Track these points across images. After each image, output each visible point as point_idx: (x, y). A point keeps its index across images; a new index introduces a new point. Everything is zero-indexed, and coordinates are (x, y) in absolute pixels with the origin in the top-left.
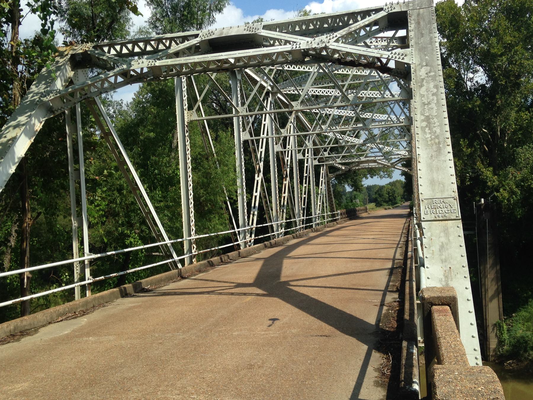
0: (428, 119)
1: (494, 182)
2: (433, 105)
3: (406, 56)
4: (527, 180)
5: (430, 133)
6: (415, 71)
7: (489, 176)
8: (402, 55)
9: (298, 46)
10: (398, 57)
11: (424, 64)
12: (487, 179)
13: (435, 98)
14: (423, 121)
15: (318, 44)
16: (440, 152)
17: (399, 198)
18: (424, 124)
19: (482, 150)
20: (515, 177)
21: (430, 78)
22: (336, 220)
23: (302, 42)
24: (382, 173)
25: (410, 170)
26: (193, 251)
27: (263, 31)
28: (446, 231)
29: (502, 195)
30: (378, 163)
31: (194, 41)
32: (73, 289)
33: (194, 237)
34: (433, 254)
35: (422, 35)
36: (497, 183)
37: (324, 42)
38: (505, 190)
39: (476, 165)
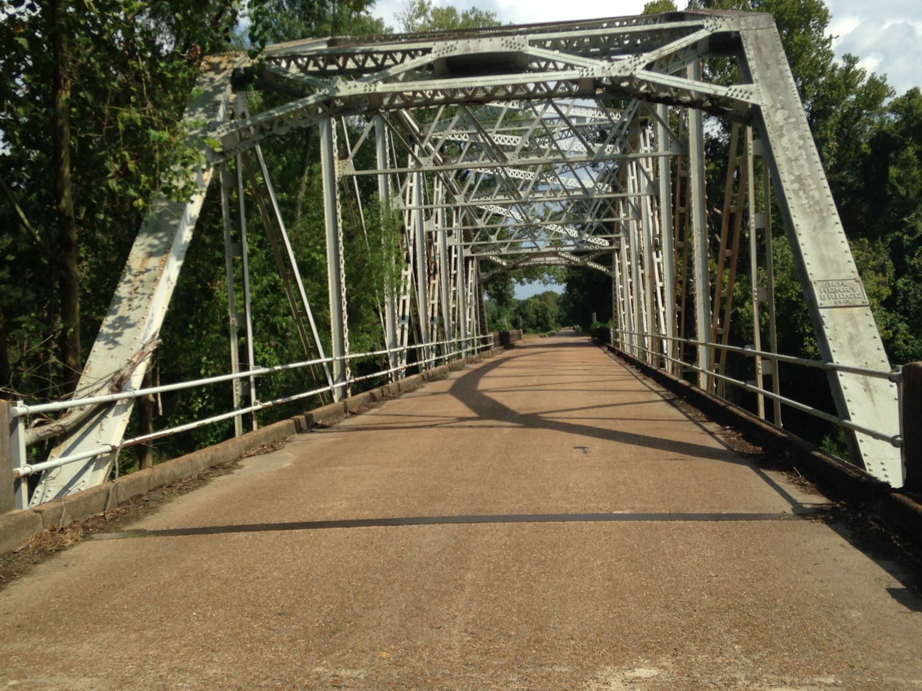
0: (799, 179)
2: (803, 162)
3: (751, 93)
5: (807, 198)
6: (768, 115)
8: (746, 92)
9: (590, 74)
10: (740, 95)
11: (779, 106)
13: (804, 153)
14: (793, 182)
15: (620, 72)
16: (824, 223)
17: (552, 321)
18: (796, 186)
21: (792, 126)
22: (487, 348)
23: (595, 67)
24: (546, 276)
25: (611, 270)
26: (348, 378)
27: (530, 48)
28: (852, 319)
30: (560, 256)
31: (429, 58)
32: (232, 419)
33: (254, 371)
34: (841, 346)
35: (768, 67)
37: (627, 69)
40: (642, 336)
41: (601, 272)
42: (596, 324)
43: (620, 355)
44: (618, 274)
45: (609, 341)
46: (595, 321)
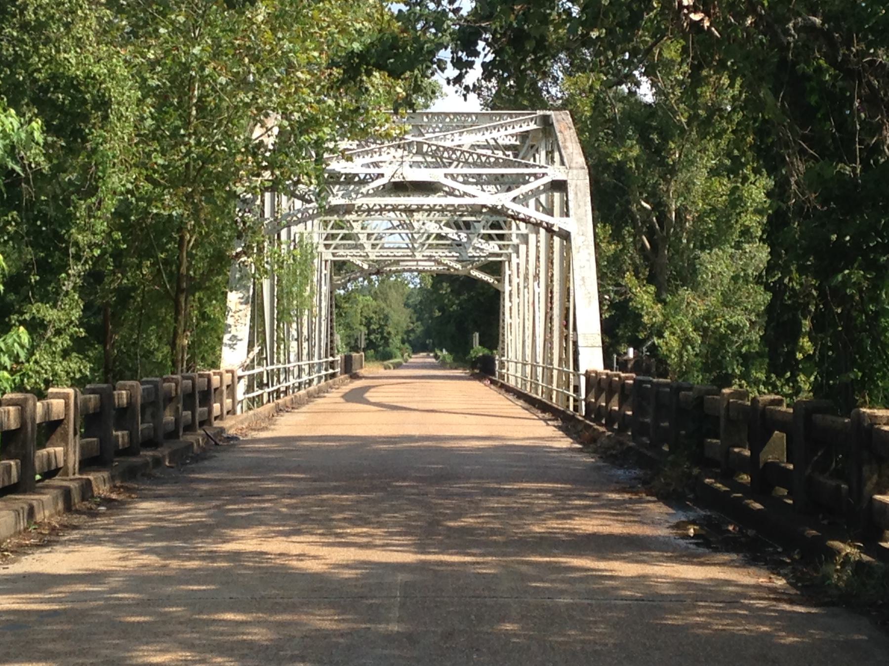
1: (655, 316)
4: (716, 317)
7: (647, 303)
12: (642, 309)
17: (395, 341)
19: (639, 246)
20: (694, 310)
22: (333, 376)
25: (499, 281)
29: (667, 343)
36: (660, 318)
38: (673, 334)
39: (623, 278)
40: (534, 367)
41: (487, 283)
42: (478, 350)
43: (508, 390)
44: (507, 288)
45: (494, 375)
46: (125, 396)
